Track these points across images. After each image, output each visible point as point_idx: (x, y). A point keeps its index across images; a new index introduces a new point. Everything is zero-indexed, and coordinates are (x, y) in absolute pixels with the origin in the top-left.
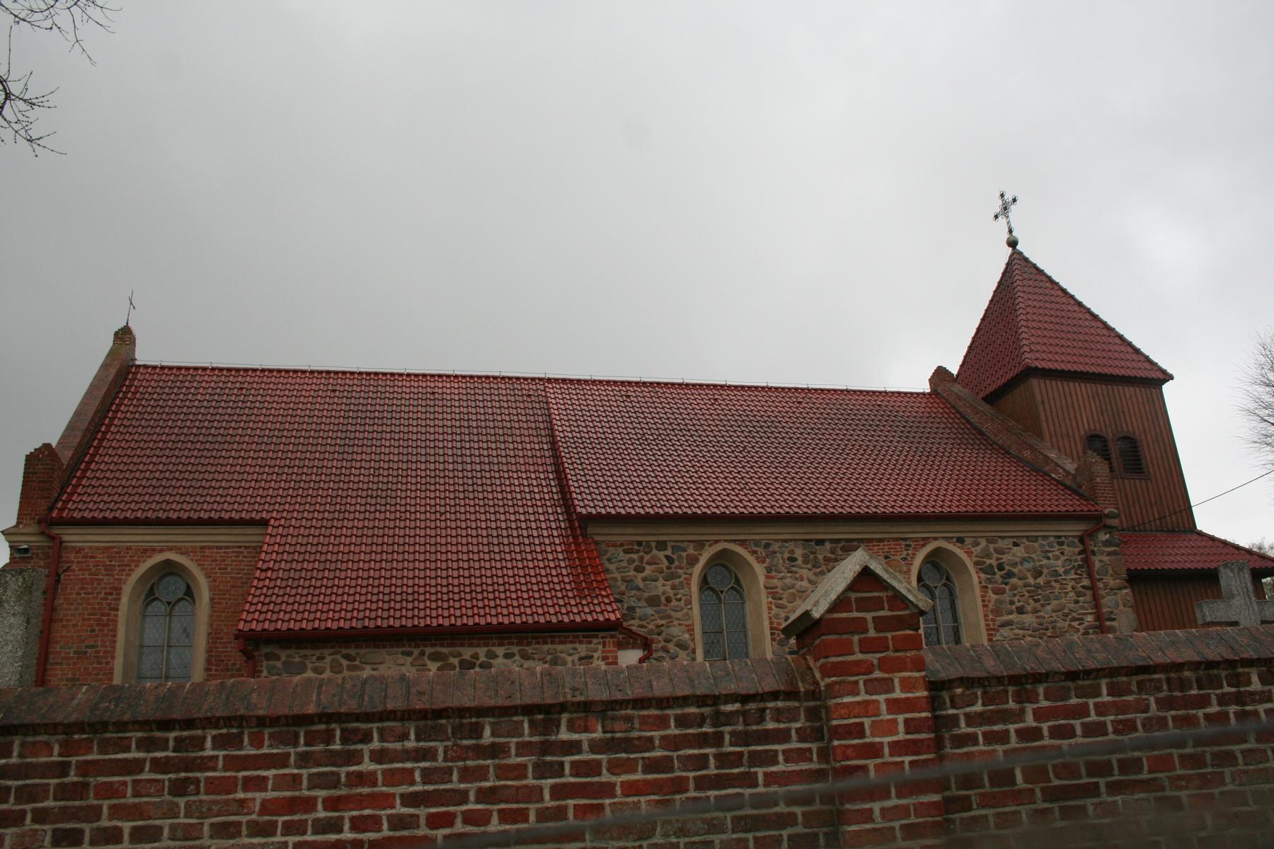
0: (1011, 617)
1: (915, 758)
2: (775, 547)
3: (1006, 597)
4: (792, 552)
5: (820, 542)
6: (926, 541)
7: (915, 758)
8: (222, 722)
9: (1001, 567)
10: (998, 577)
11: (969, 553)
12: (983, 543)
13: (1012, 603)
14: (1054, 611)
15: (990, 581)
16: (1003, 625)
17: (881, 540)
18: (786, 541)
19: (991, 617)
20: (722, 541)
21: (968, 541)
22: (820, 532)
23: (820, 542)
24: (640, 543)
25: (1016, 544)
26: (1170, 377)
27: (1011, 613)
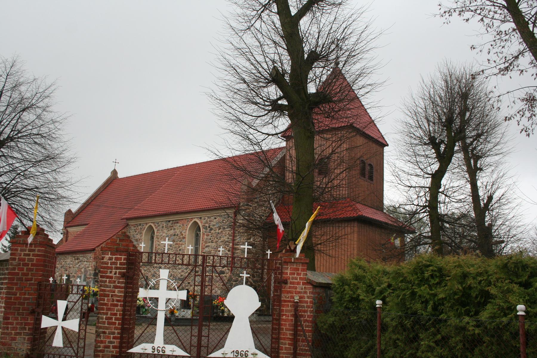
0: (209, 244)
1: (9, 291)
2: (159, 224)
3: (209, 237)
4: (163, 225)
5: (169, 221)
6: (147, 224)
7: (9, 291)
8: (37, 322)
9: (209, 227)
10: (208, 230)
11: (201, 222)
12: (206, 218)
13: (210, 239)
14: (221, 242)
15: (205, 232)
16: (206, 247)
17: (182, 220)
18: (162, 222)
19: (204, 244)
20: (150, 223)
21: (203, 218)
22: (172, 218)
23: (169, 221)
24: (136, 224)
25: (215, 218)
26: (387, 145)
27: (209, 243)
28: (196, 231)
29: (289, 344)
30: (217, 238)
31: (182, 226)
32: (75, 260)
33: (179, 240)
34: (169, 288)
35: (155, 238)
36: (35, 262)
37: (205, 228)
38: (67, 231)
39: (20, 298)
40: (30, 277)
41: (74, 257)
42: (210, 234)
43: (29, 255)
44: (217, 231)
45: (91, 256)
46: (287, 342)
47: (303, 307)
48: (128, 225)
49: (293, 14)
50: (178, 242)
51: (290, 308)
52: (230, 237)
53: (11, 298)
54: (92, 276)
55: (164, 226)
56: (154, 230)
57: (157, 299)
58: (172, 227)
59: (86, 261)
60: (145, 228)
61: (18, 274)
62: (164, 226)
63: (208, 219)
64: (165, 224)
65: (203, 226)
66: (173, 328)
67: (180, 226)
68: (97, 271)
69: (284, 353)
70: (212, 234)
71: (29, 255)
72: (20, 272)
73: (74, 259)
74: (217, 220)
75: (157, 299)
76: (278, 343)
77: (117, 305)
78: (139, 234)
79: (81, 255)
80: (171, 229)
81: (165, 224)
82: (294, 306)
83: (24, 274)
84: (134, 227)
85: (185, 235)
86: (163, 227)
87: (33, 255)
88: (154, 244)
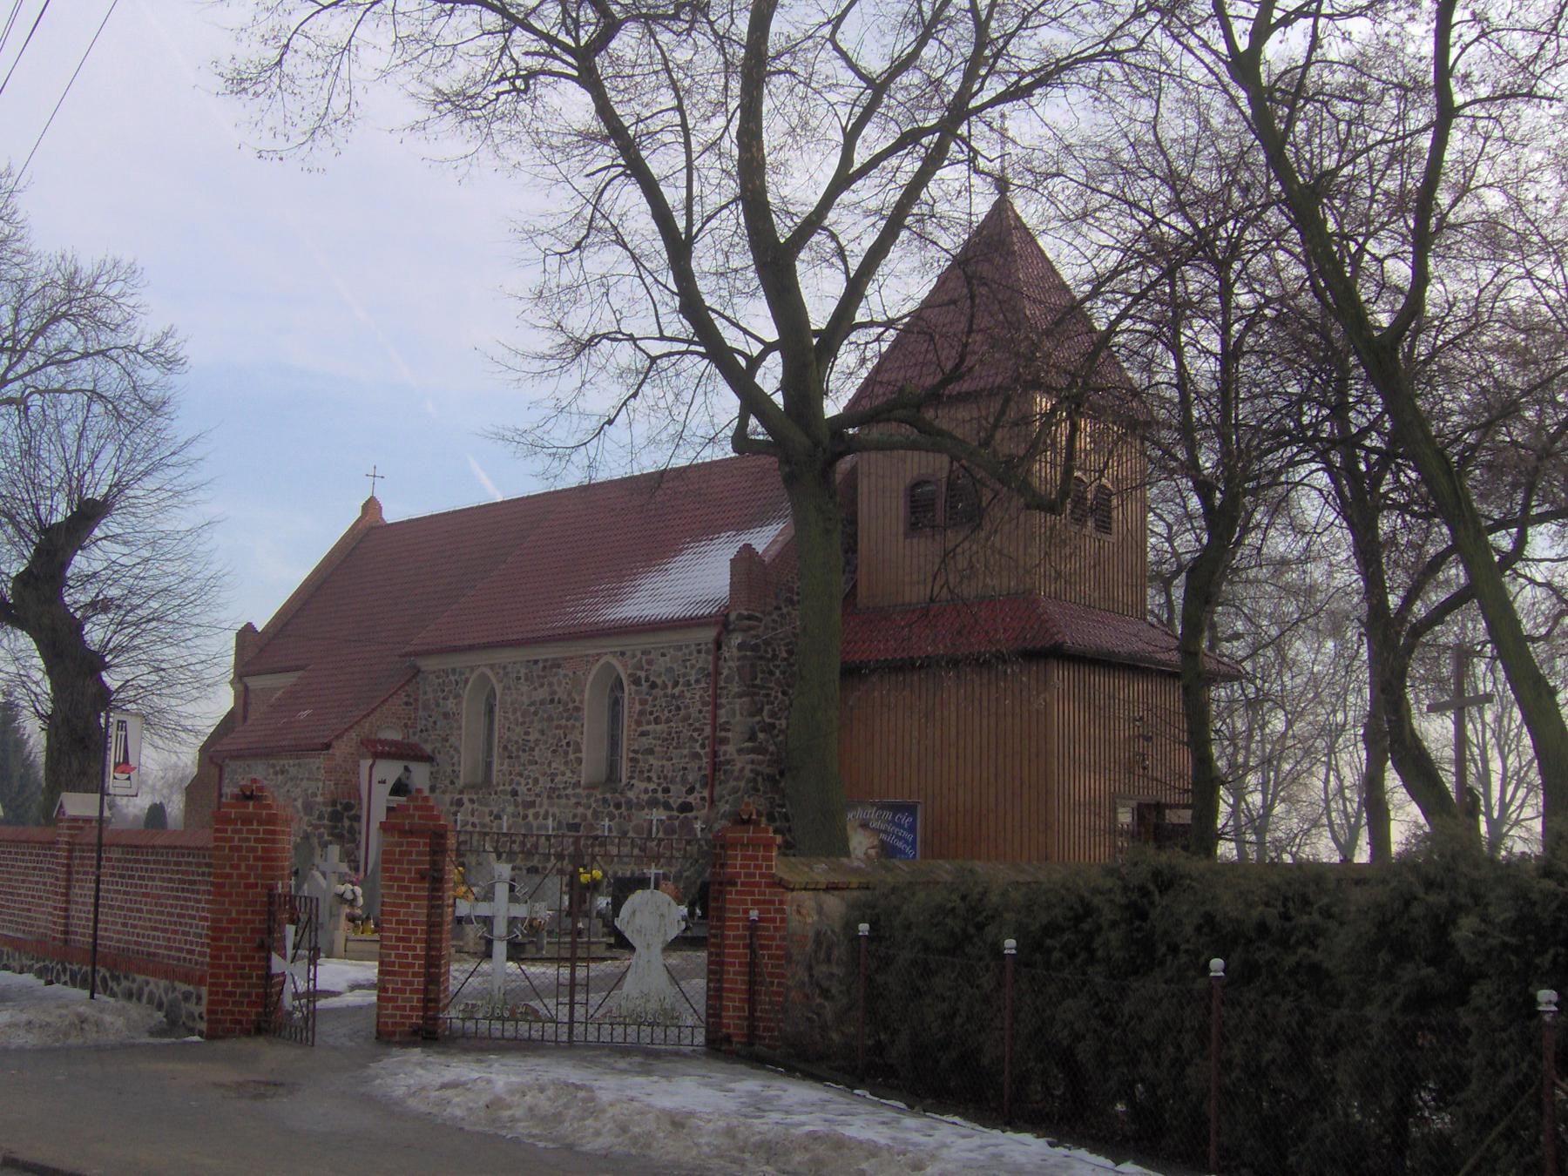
5: (536, 662)
6: (472, 669)
9: (647, 680)
11: (625, 666)
25: (663, 655)
28: (612, 690)
29: (741, 1000)
30: (670, 711)
31: (571, 675)
32: (276, 773)
33: (565, 715)
34: (512, 921)
35: (497, 709)
36: (260, 853)
37: (636, 681)
38: (246, 688)
39: (238, 921)
40: (252, 880)
41: (274, 766)
42: (650, 699)
43: (248, 840)
44: (669, 691)
45: (317, 763)
46: (737, 996)
47: (768, 929)
48: (417, 672)
49: (752, 416)
50: (563, 722)
51: (741, 932)
52: (705, 709)
53: (220, 920)
54: (326, 822)
55: (522, 675)
56: (493, 690)
57: (491, 899)
58: (545, 677)
59: (308, 779)
60: (467, 681)
61: (229, 876)
62: (522, 675)
63: (644, 658)
64: (523, 671)
65: (630, 675)
66: (1297, 67)
67: (566, 676)
68: (339, 807)
69: (730, 1017)
70: (655, 699)
71: (248, 840)
72: (235, 872)
73: (271, 771)
74: (667, 658)
75: (491, 899)
76: (720, 998)
77: (415, 932)
78: (451, 700)
79: (291, 762)
80: (542, 685)
81: (523, 671)
82: (745, 928)
83: (241, 876)
84: (438, 677)
85: (581, 702)
86: (519, 678)
87: (256, 840)
88: (496, 726)
